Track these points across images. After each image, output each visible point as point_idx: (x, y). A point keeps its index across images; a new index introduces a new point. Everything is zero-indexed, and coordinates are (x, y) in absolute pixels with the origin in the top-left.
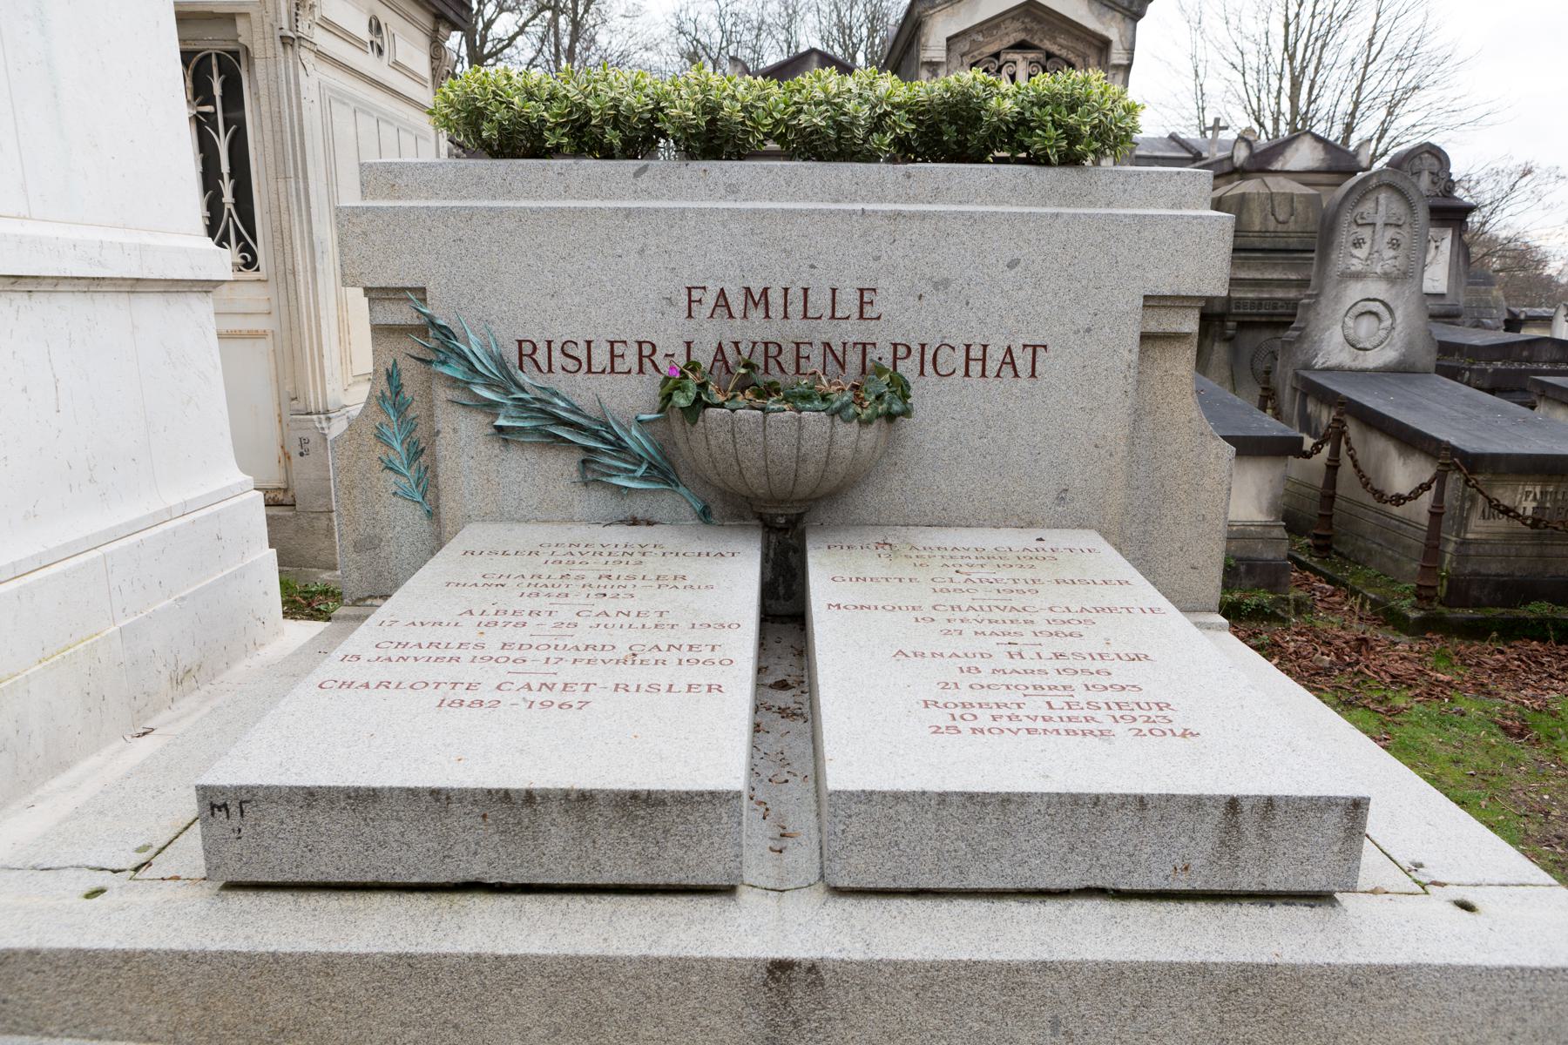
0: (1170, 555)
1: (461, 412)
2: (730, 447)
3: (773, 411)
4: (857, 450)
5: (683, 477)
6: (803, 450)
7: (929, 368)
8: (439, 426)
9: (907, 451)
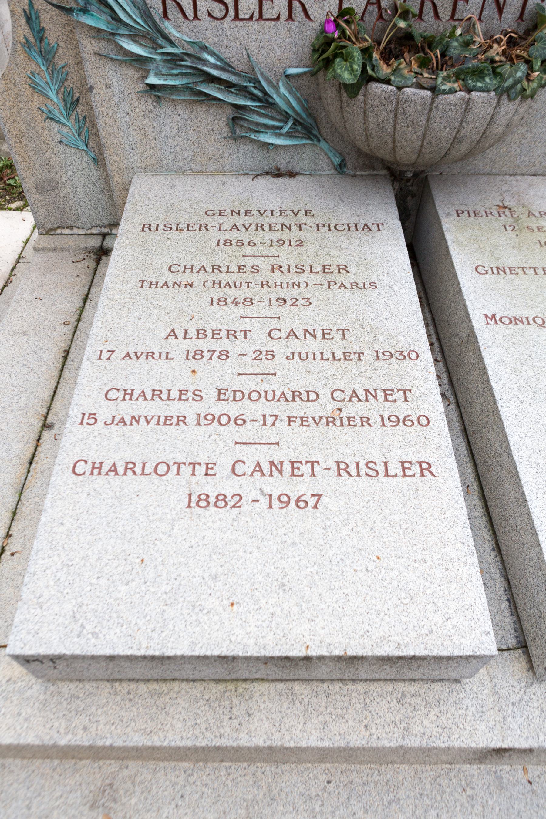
1: (109, 66)
2: (389, 127)
3: (444, 92)
5: (324, 131)
6: (463, 132)
8: (91, 81)
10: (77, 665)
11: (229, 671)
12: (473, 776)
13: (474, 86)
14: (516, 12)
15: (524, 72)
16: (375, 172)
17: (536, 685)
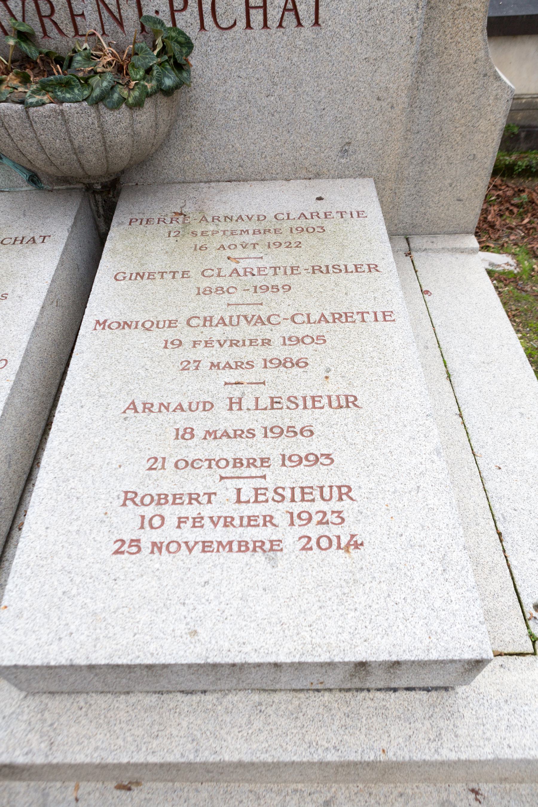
0: (441, 190)
3: (32, 105)
4: (135, 134)
6: (76, 143)
7: (208, 20)
9: (200, 114)
10: (57, 670)
11: (359, 676)
12: (19, 793)
13: (64, 97)
14: (136, 25)
15: (109, 82)
16: (72, 186)
17: (30, 698)
